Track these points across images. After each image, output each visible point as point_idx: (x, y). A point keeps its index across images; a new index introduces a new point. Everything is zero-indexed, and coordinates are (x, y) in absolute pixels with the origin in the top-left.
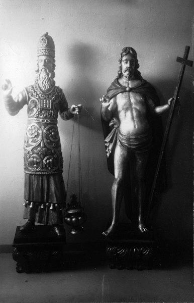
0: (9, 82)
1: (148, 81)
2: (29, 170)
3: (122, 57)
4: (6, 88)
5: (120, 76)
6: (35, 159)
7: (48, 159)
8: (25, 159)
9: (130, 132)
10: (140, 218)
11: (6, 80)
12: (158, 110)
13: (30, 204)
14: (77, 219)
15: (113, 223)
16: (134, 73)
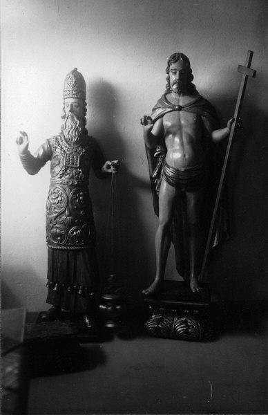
0: (24, 134)
1: (204, 97)
2: (52, 244)
3: (169, 66)
4: (21, 142)
5: (169, 91)
6: (58, 231)
7: (75, 230)
8: (49, 228)
9: (192, 135)
10: (167, 302)
11: (21, 132)
12: (217, 135)
13: (54, 287)
14: (114, 309)
15: (157, 279)
16: (185, 84)
